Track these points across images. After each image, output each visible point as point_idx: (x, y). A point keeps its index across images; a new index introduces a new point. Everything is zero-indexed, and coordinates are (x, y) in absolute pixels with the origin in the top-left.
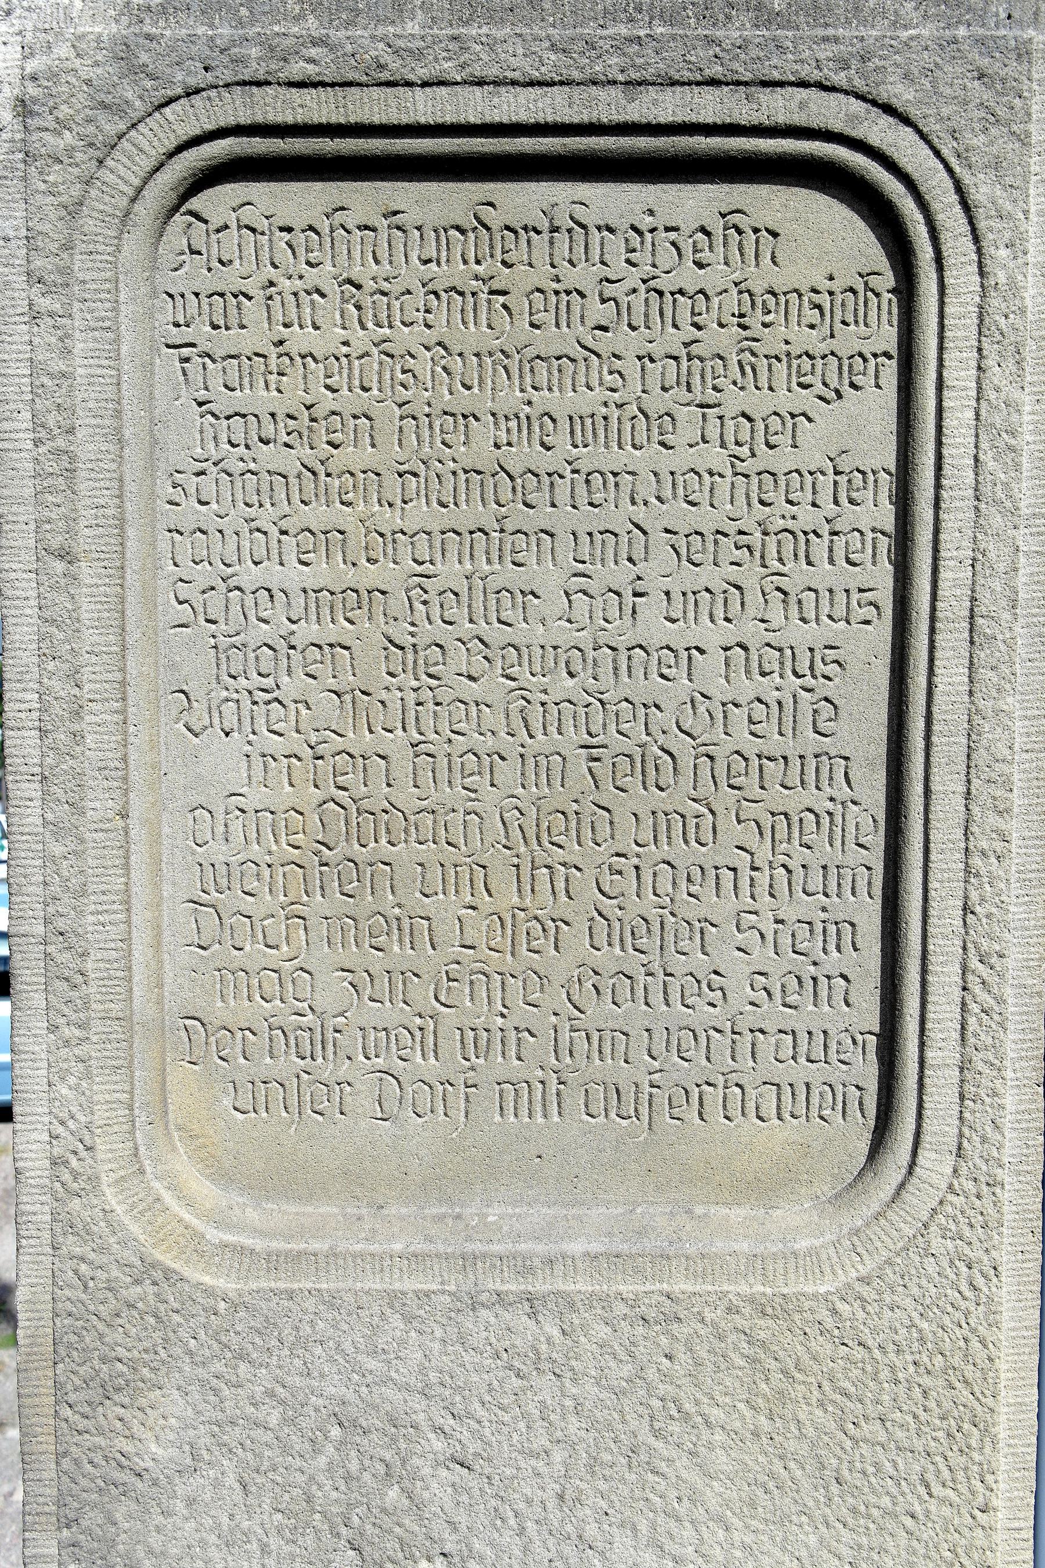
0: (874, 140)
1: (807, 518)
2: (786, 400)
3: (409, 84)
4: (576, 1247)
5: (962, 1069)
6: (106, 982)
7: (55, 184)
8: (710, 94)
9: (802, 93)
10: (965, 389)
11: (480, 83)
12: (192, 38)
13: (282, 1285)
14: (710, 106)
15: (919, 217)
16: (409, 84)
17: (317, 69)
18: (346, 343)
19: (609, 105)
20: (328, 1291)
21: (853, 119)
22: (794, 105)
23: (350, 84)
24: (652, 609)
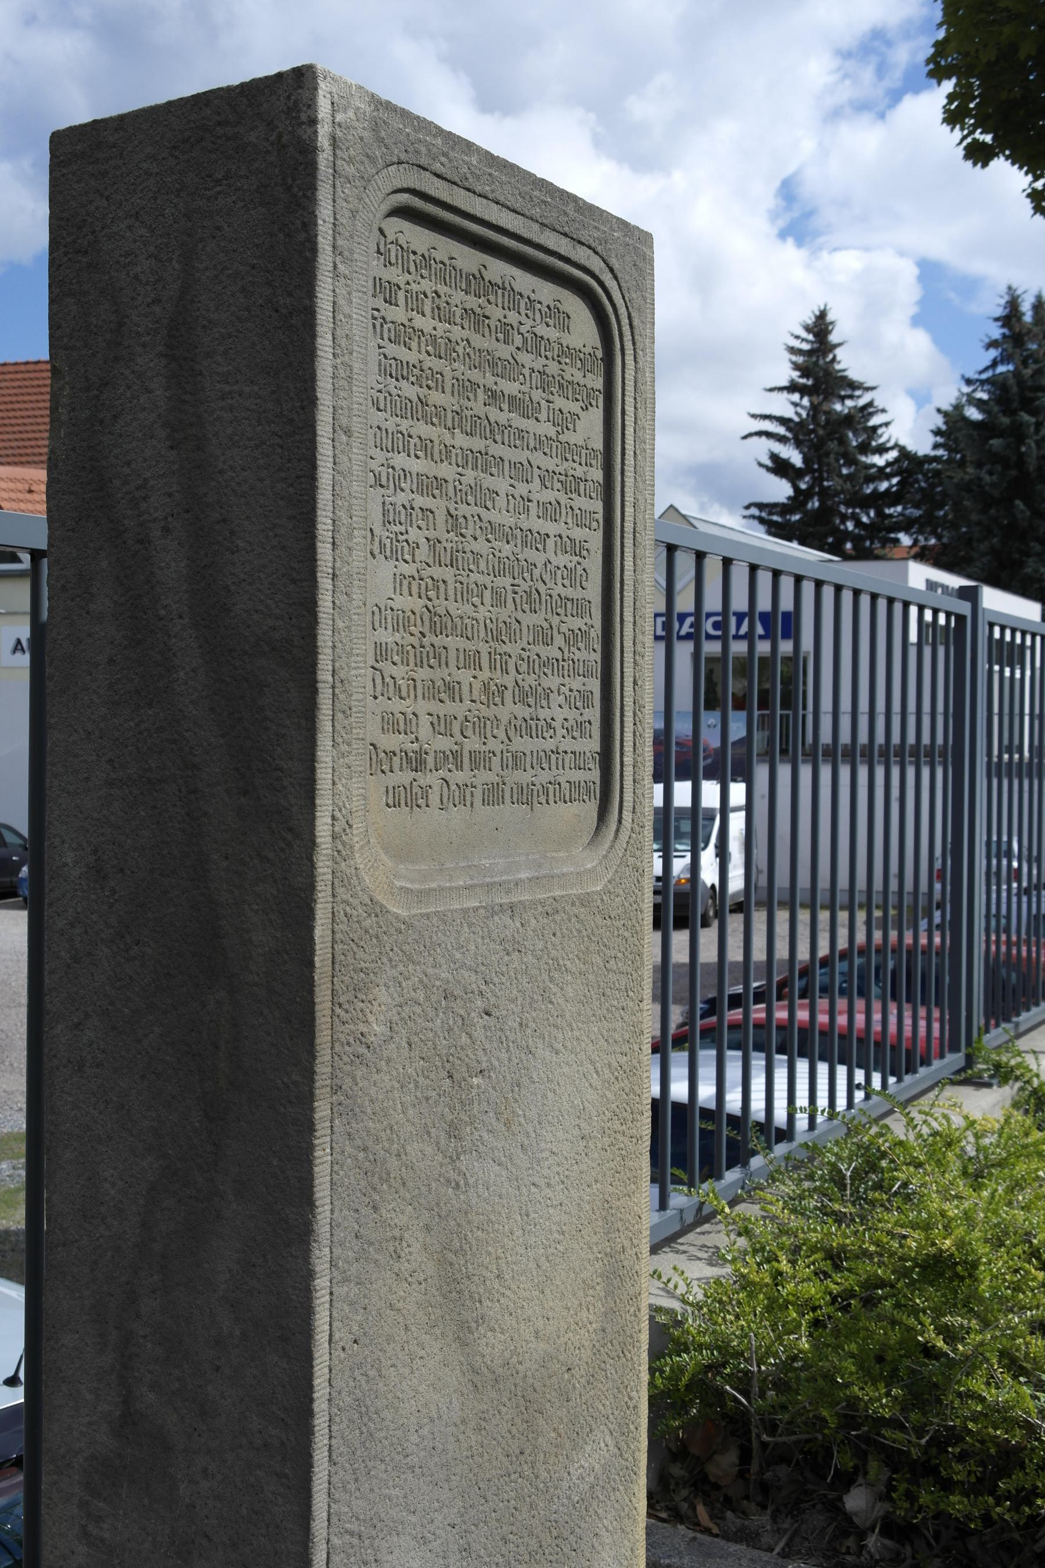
4: (523, 875)
5: (634, 766)
7: (348, 196)
8: (565, 241)
11: (497, 203)
12: (400, 131)
13: (423, 911)
14: (563, 246)
18: (435, 329)
21: (601, 269)
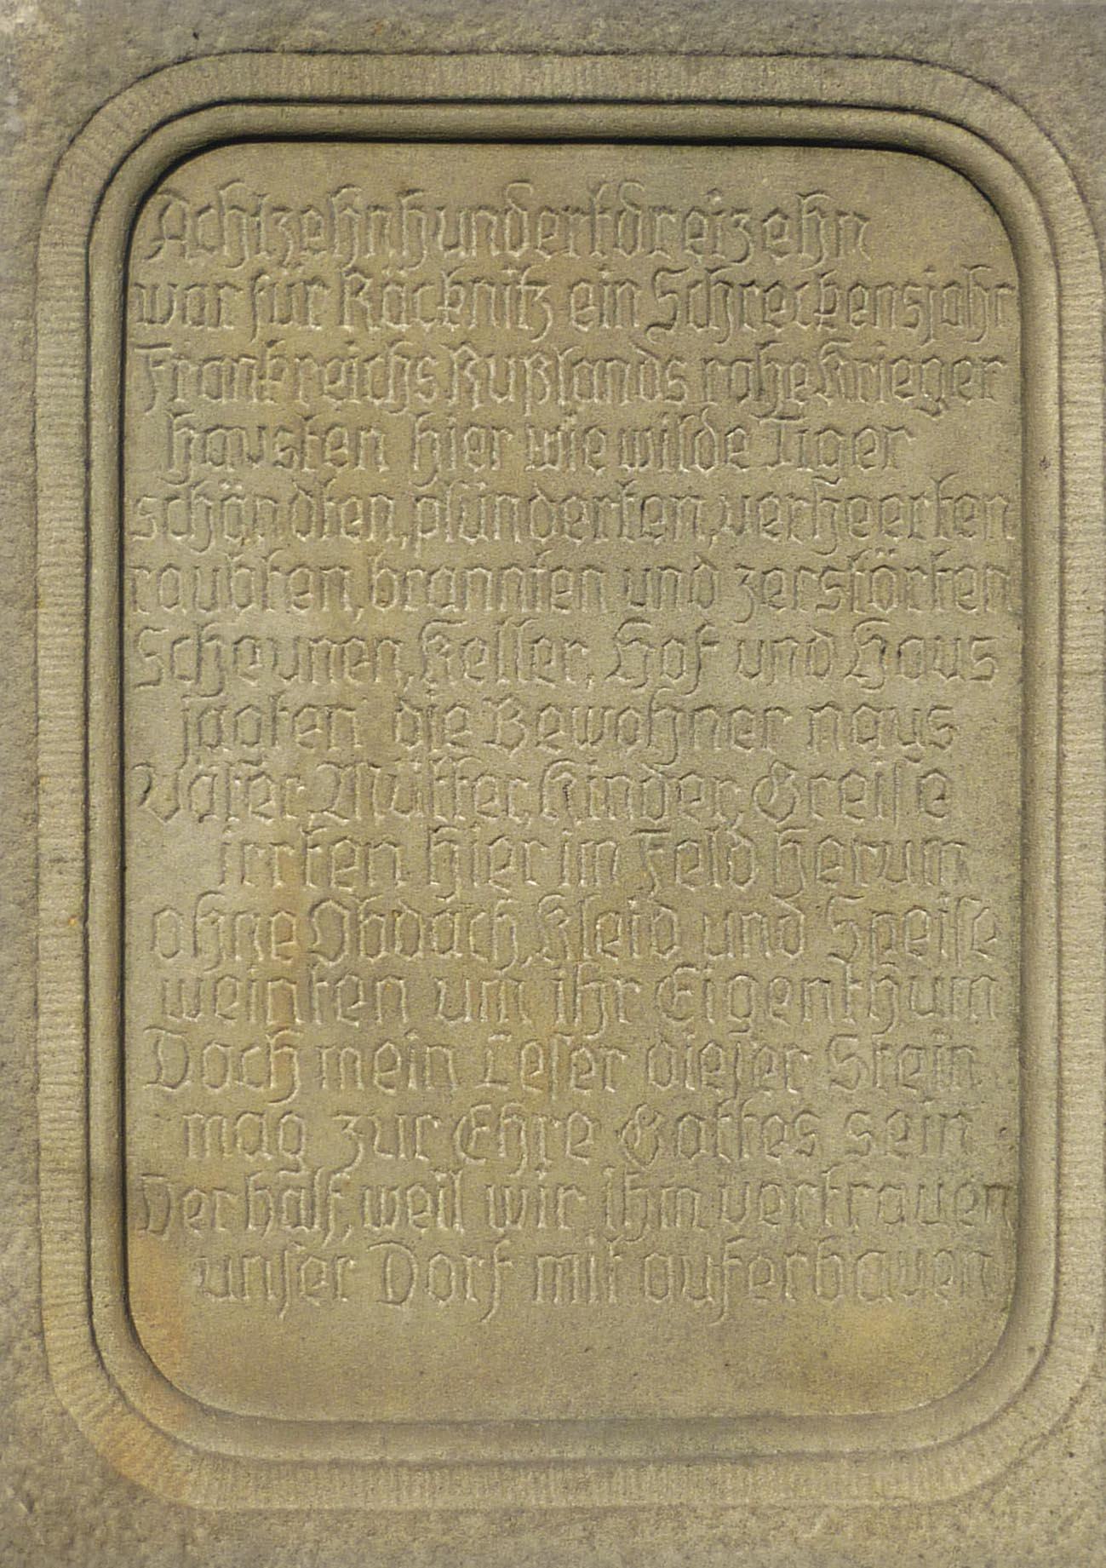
0: (976, 119)
1: (907, 550)
2: (882, 409)
3: (434, 52)
6: (56, 1125)
9: (895, 65)
10: (1089, 404)
14: (786, 79)
15: (1032, 206)
16: (434, 52)
17: (329, 37)
19: (670, 78)
20: (331, 1511)
22: (107, 134)
23: (366, 52)
24: (721, 659)
